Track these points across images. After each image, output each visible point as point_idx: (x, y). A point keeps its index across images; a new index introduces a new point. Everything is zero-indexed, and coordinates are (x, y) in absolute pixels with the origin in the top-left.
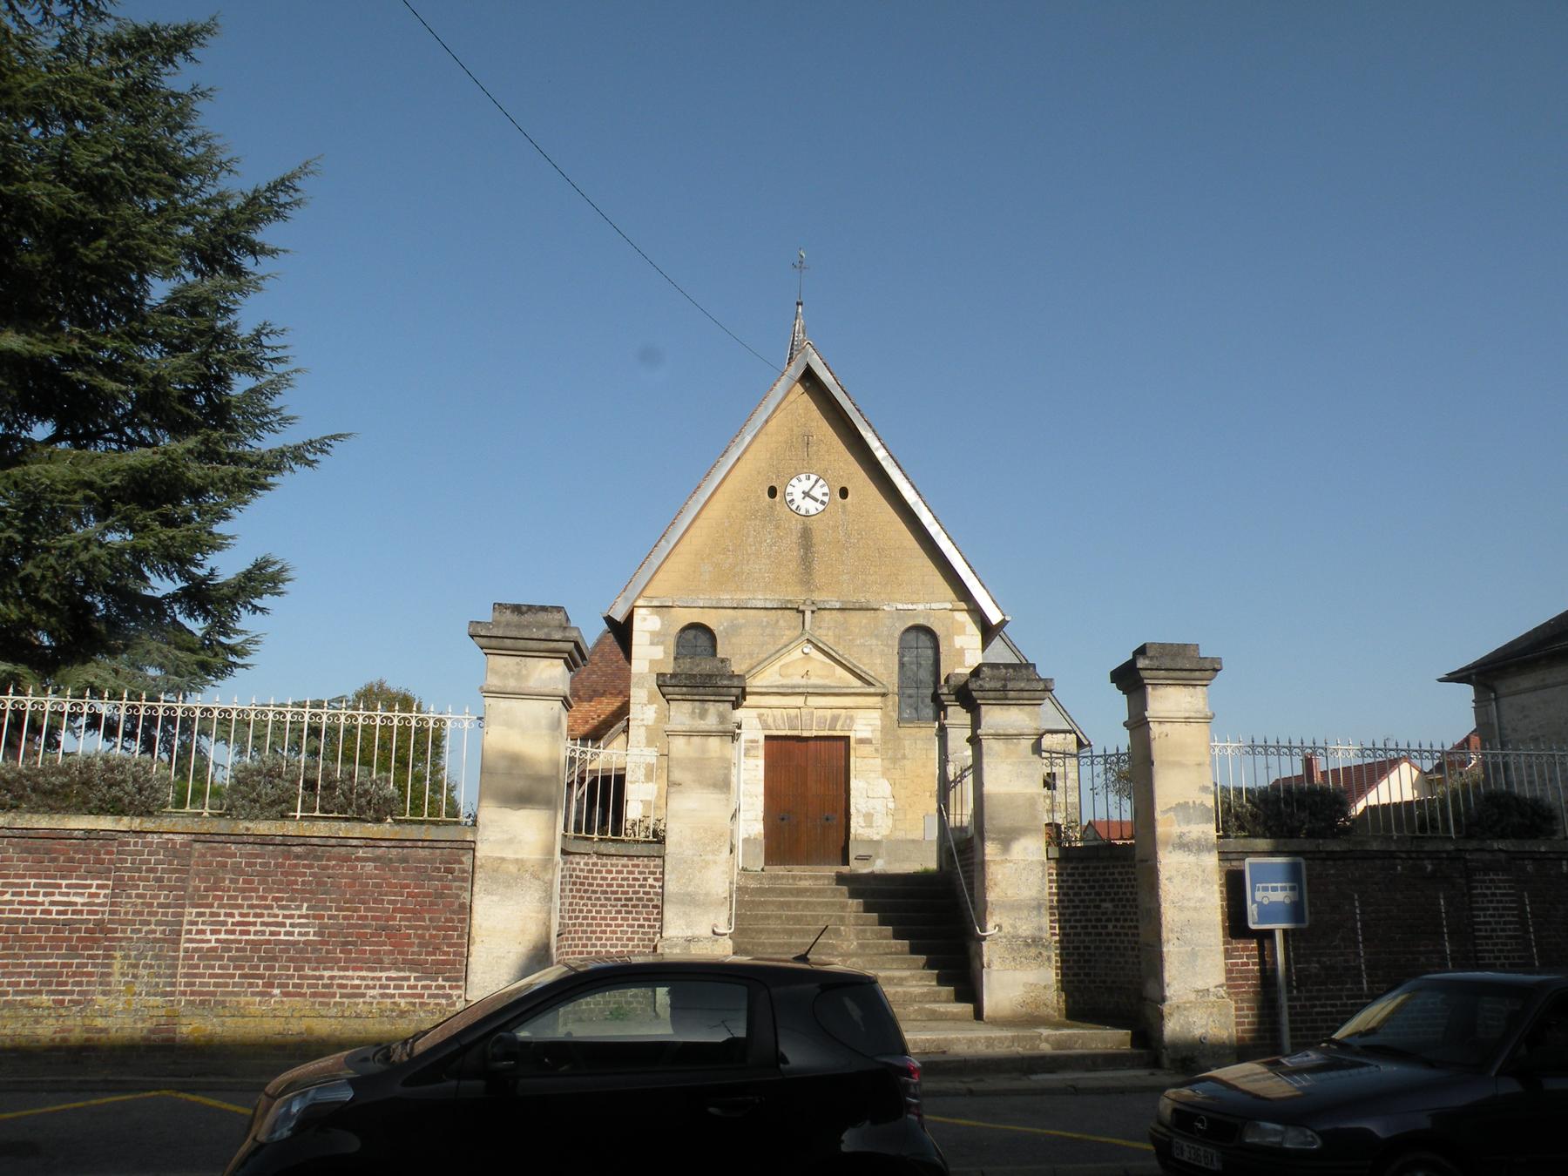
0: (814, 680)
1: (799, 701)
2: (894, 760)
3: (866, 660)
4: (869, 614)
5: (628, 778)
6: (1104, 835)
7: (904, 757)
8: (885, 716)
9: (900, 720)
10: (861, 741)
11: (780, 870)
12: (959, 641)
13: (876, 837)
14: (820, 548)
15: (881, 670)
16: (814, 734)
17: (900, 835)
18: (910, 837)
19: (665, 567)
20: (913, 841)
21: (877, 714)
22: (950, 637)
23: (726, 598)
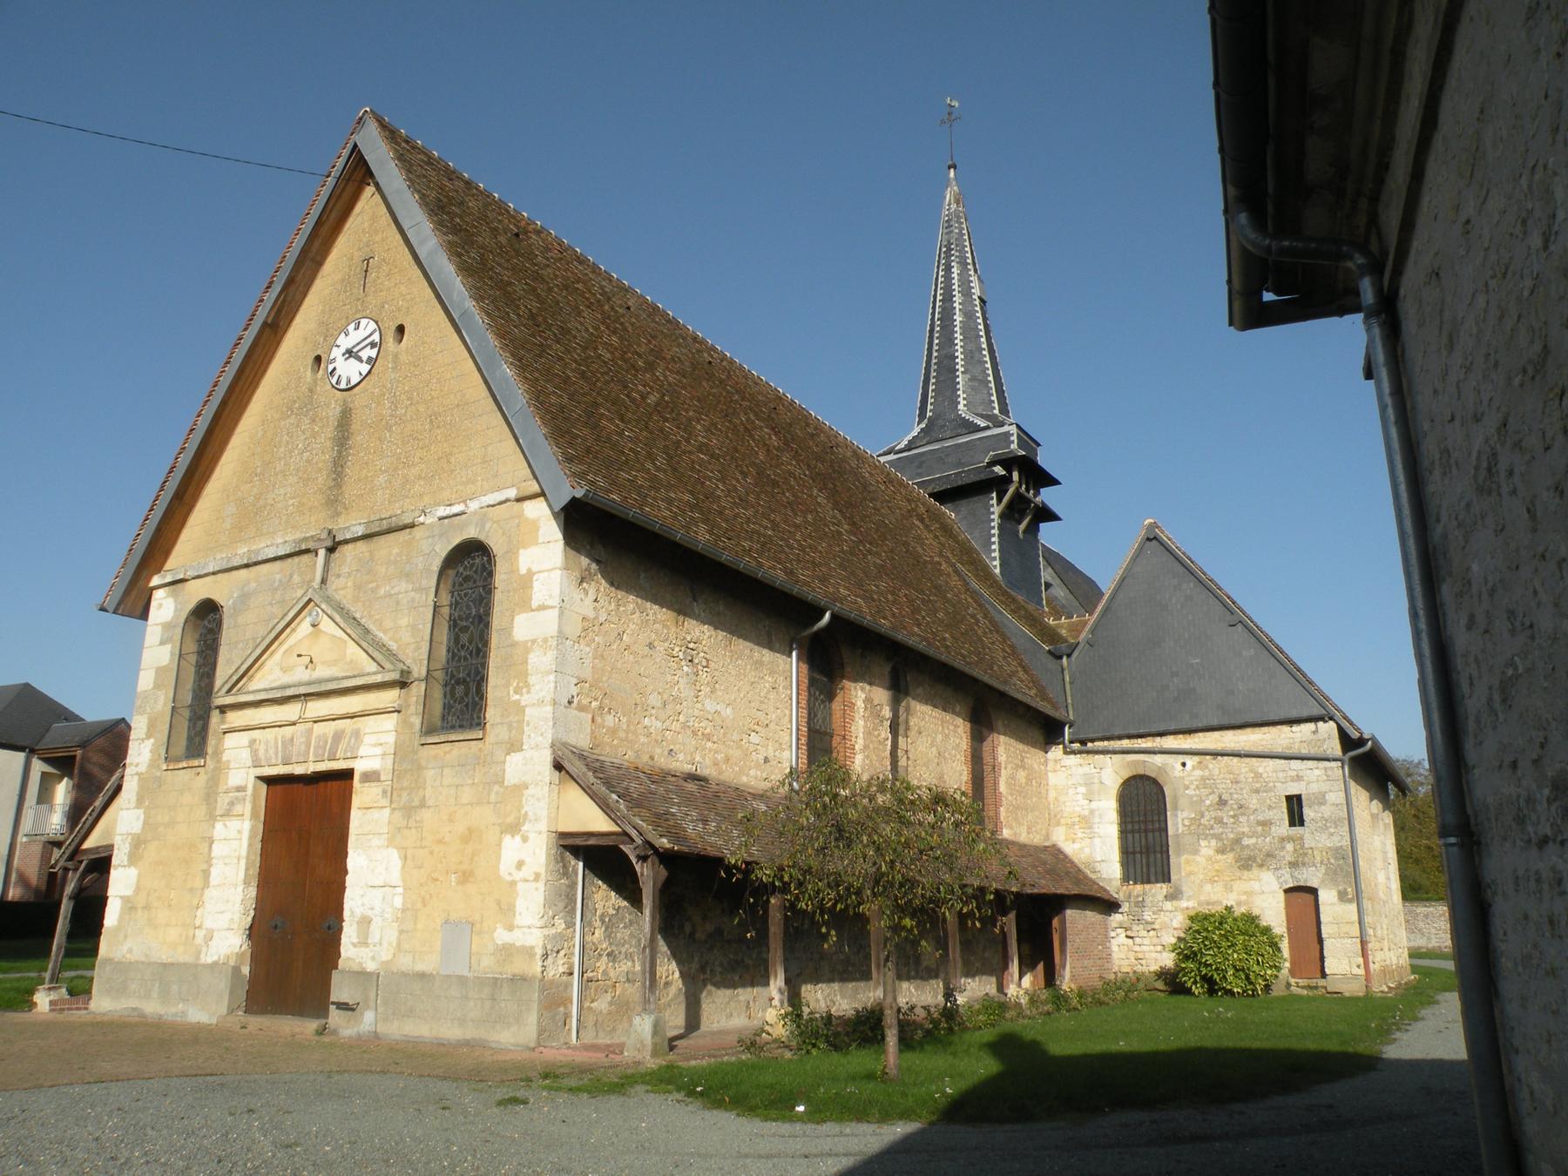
0: (321, 672)
1: (291, 711)
2: (409, 811)
3: (388, 623)
4: (403, 536)
5: (114, 861)
6: (669, 970)
7: (423, 805)
8: (406, 723)
9: (429, 730)
10: (370, 777)
11: (257, 1022)
12: (527, 559)
13: (371, 967)
14: (359, 438)
15: (406, 637)
16: (311, 768)
17: (406, 963)
18: (420, 967)
19: (1212, 600)
20: (422, 976)
21: (390, 722)
22: (512, 554)
23: (242, 553)
